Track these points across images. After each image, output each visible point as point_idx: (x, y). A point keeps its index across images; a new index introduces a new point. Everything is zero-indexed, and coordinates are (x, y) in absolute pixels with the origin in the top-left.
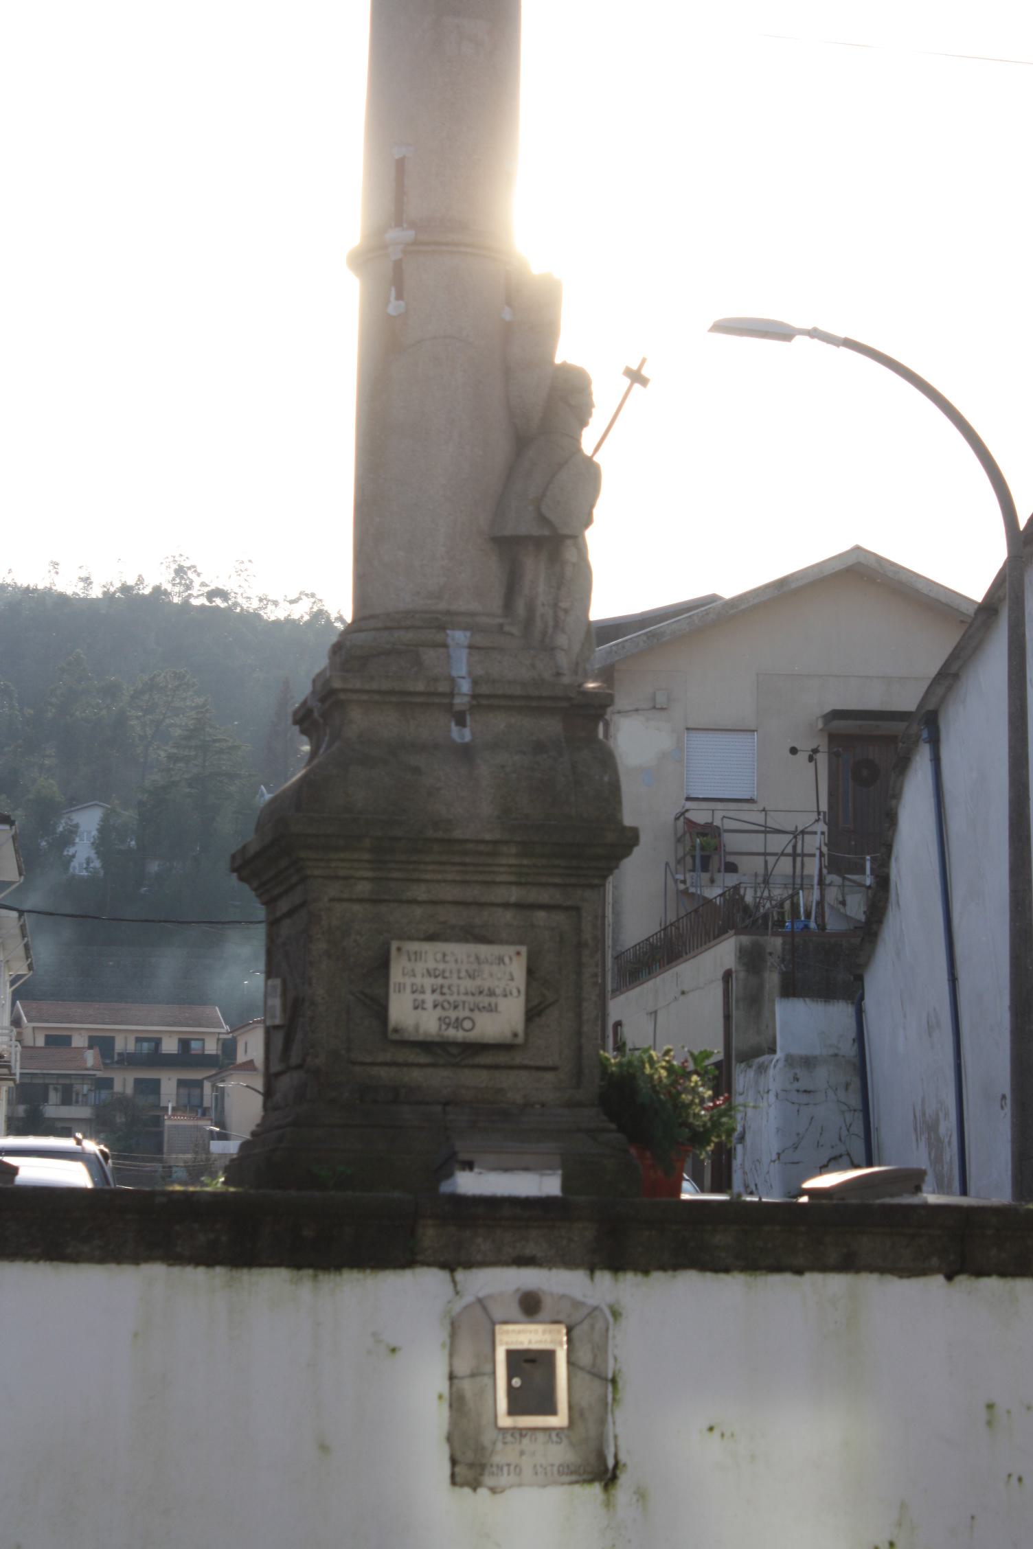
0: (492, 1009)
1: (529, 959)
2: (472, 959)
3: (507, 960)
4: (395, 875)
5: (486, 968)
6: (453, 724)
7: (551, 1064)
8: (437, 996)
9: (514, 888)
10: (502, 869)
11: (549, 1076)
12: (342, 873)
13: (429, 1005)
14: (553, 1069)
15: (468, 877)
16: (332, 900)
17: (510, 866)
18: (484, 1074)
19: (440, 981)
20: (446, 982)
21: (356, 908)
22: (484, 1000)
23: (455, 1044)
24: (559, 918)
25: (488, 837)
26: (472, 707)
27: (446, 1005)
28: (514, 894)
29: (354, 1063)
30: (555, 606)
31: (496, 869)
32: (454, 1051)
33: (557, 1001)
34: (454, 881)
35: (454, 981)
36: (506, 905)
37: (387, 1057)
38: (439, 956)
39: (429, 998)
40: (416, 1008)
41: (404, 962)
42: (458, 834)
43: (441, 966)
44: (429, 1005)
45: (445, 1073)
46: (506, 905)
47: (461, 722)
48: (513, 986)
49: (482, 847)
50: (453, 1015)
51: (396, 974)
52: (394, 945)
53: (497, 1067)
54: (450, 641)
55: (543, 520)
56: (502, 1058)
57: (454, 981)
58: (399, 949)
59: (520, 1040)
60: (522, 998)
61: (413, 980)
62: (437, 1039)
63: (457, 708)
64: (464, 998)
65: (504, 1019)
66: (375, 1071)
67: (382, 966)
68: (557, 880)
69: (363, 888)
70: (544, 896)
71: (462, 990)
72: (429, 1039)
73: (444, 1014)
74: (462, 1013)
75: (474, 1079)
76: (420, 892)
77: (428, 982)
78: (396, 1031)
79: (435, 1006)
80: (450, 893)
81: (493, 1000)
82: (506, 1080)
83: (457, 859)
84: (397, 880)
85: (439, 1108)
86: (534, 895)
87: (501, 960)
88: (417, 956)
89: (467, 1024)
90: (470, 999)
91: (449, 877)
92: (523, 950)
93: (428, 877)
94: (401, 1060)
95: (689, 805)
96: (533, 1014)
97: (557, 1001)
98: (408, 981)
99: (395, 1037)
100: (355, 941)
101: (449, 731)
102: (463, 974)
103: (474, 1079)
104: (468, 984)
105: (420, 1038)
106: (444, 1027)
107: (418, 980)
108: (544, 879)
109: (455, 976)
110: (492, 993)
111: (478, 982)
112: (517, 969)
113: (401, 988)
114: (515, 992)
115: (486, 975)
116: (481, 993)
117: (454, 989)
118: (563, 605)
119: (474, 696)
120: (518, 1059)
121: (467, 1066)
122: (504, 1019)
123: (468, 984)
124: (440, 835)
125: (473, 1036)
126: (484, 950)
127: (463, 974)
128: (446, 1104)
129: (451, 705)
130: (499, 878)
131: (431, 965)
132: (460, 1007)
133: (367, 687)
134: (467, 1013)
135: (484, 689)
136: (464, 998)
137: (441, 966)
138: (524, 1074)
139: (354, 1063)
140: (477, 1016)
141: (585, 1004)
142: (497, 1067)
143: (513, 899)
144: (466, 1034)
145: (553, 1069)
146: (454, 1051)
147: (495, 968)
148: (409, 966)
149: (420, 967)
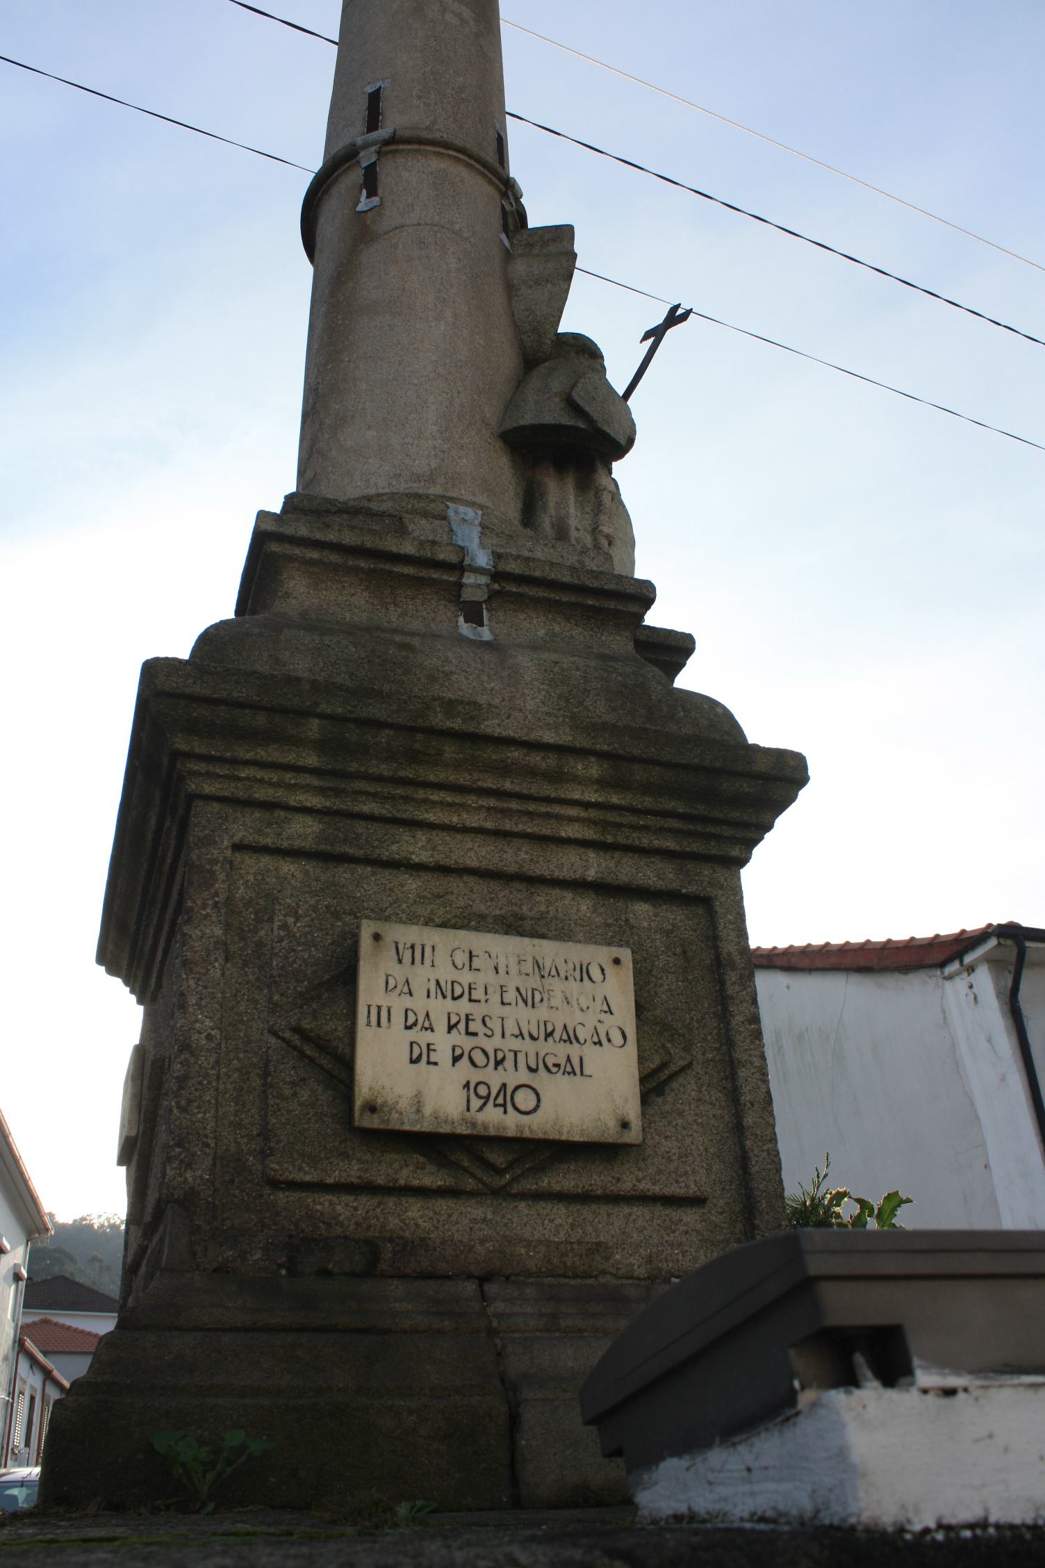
0: (574, 1069)
1: (637, 973)
2: (528, 967)
3: (595, 973)
4: (368, 807)
5: (557, 985)
6: (461, 619)
7: (693, 1190)
8: (458, 1038)
9: (591, 855)
10: (573, 812)
11: (690, 1217)
12: (261, 794)
13: (443, 1055)
14: (697, 1201)
15: (508, 825)
16: (238, 847)
17: (587, 805)
18: (560, 1214)
19: (464, 1006)
20: (477, 1011)
21: (288, 867)
22: (557, 1051)
23: (501, 1141)
24: (675, 916)
25: (549, 737)
26: (493, 595)
27: (479, 1057)
28: (594, 866)
29: (275, 1184)
30: (595, 530)
31: (557, 809)
32: (499, 1159)
33: (689, 1065)
34: (480, 831)
35: (495, 1009)
36: (579, 886)
37: (351, 1171)
38: (461, 958)
39: (443, 1042)
40: (414, 1061)
41: (387, 963)
42: (491, 726)
43: (466, 978)
44: (443, 1055)
45: (476, 1211)
46: (579, 886)
47: (474, 617)
48: (610, 1024)
49: (536, 759)
50: (495, 1079)
51: (371, 989)
52: (367, 930)
53: (585, 1198)
54: (451, 513)
55: (573, 406)
56: (595, 1178)
57: (495, 1009)
58: (377, 937)
59: (634, 1135)
60: (632, 1049)
61: (407, 1002)
62: (462, 1130)
63: (467, 595)
64: (516, 1044)
65: (596, 1092)
66: (323, 1203)
67: (344, 977)
68: (670, 844)
69: (303, 830)
70: (649, 874)
71: (511, 1028)
72: (446, 1129)
73: (475, 1076)
74: (513, 1076)
75: (538, 1226)
76: (417, 847)
77: (440, 1009)
78: (372, 1108)
79: (456, 1059)
80: (475, 853)
81: (574, 1051)
82: (608, 1225)
83: (489, 783)
84: (371, 818)
85: (470, 1288)
86: (628, 870)
87: (584, 973)
88: (417, 954)
89: (525, 1100)
90: (527, 1046)
91: (473, 820)
92: (626, 954)
93: (431, 817)
94: (381, 1181)
95: (507, 1034)
96: (653, 1085)
97: (689, 1065)
98: (398, 1004)
99: (372, 1122)
100: (284, 926)
101: (457, 627)
102: (511, 996)
103: (538, 1226)
104: (522, 1016)
105: (426, 1126)
106: (476, 1103)
107: (419, 1003)
108: (645, 841)
109: (495, 998)
110: (571, 1037)
111: (542, 1013)
112: (618, 990)
113: (381, 1017)
114: (617, 1038)
115: (557, 1001)
116: (549, 1035)
117: (495, 1025)
118: (605, 529)
119: (497, 575)
120: (629, 1179)
121: (523, 1196)
122: (596, 1092)
123: (522, 1016)
124: (457, 724)
125: (537, 1125)
126: (549, 951)
127: (511, 996)
128: (484, 1279)
129: (460, 586)
130: (568, 831)
131: (445, 973)
132: (509, 1063)
133: (319, 536)
134: (523, 1076)
135: (513, 567)
136: (516, 1044)
137: (466, 978)
138: (640, 1213)
139: (275, 1184)
140: (542, 1081)
141: (742, 1073)
142: (585, 1198)
143: (591, 874)
144: (525, 1119)
145: (697, 1201)
146: (499, 1159)
147: (573, 987)
148: (399, 973)
149: (422, 977)
